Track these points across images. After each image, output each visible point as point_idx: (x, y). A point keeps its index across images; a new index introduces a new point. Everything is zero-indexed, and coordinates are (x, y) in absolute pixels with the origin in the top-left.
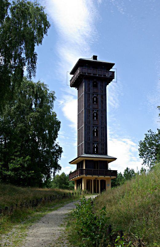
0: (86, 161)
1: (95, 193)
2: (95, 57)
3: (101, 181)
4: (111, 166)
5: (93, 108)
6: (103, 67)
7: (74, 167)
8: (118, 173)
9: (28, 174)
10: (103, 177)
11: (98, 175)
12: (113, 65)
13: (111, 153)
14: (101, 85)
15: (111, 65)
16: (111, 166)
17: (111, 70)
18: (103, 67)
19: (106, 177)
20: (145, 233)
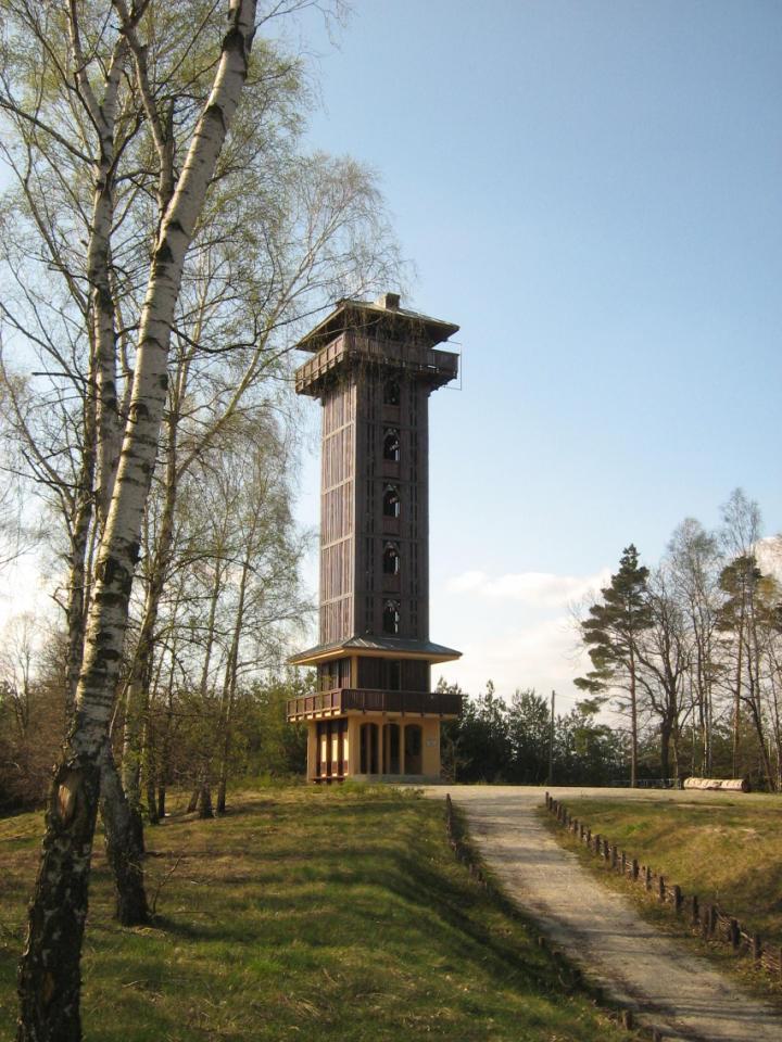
0: (360, 659)
1: (395, 769)
2: (392, 300)
3: (406, 728)
4: (441, 676)
5: (386, 478)
6: (55, 936)
7: (703, 571)
8: (565, 704)
9: (228, 865)
10: (418, 715)
11: (421, 712)
12: (452, 329)
13: (438, 635)
14: (411, 398)
15: (444, 331)
16: (441, 676)
17: (441, 347)
18: (55, 936)
19: (428, 715)
20: (216, 741)
